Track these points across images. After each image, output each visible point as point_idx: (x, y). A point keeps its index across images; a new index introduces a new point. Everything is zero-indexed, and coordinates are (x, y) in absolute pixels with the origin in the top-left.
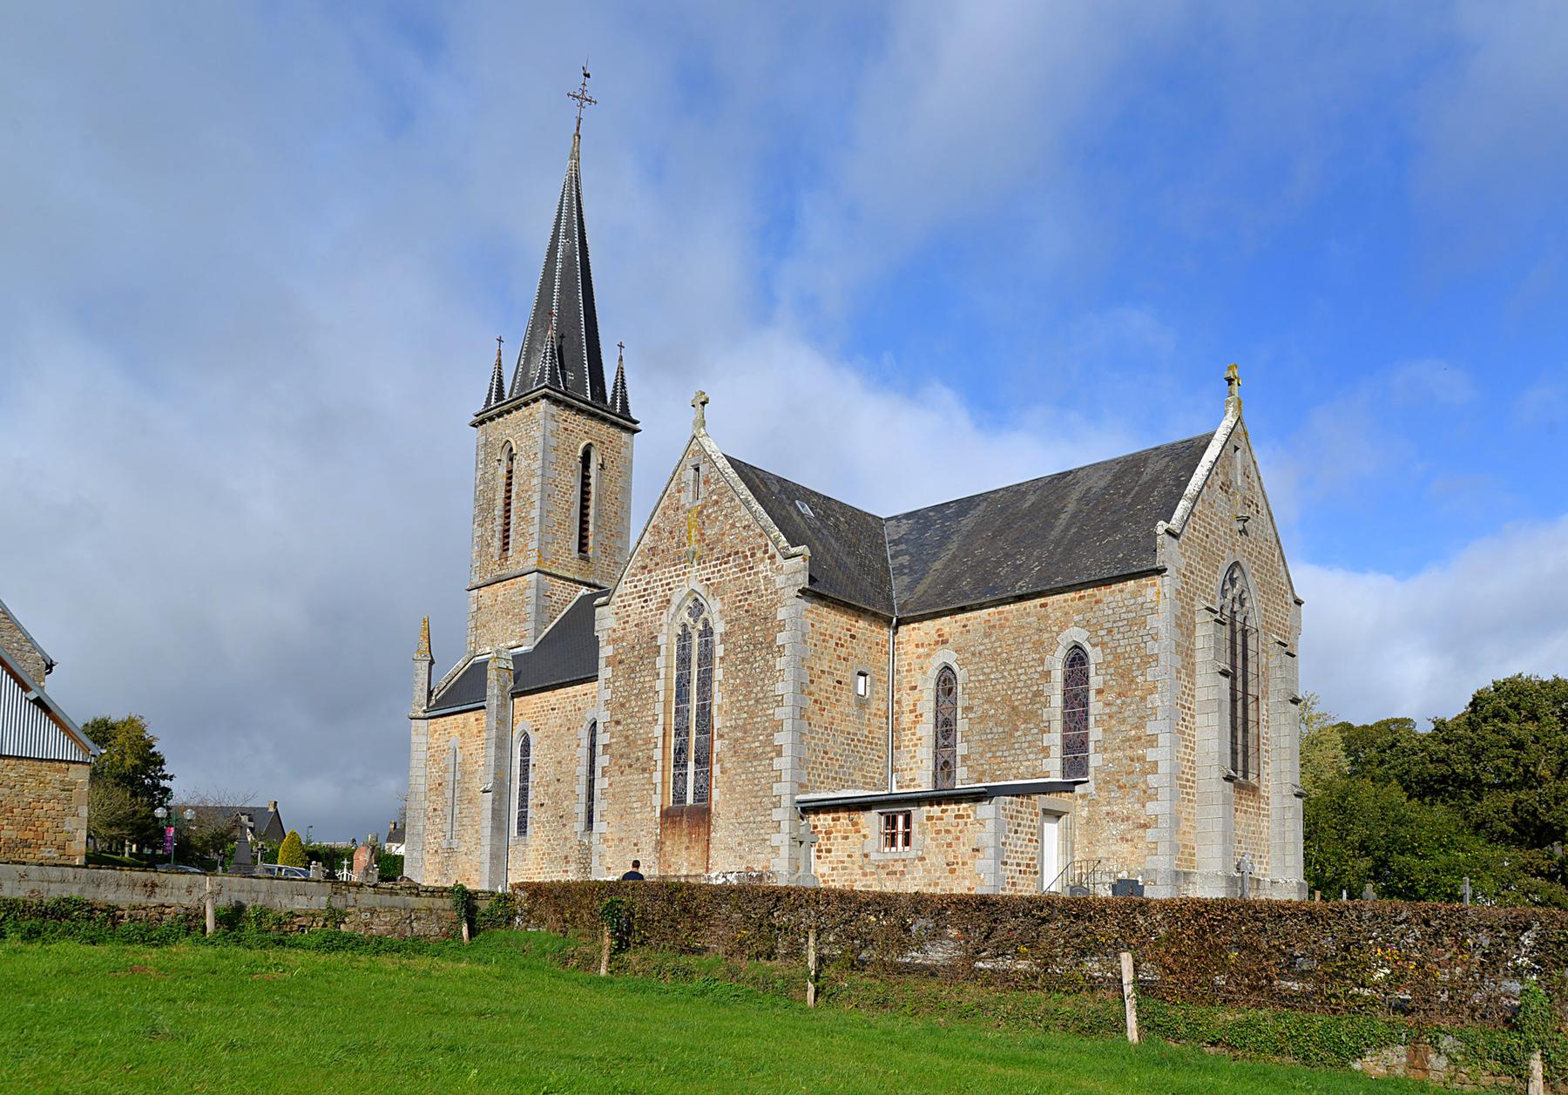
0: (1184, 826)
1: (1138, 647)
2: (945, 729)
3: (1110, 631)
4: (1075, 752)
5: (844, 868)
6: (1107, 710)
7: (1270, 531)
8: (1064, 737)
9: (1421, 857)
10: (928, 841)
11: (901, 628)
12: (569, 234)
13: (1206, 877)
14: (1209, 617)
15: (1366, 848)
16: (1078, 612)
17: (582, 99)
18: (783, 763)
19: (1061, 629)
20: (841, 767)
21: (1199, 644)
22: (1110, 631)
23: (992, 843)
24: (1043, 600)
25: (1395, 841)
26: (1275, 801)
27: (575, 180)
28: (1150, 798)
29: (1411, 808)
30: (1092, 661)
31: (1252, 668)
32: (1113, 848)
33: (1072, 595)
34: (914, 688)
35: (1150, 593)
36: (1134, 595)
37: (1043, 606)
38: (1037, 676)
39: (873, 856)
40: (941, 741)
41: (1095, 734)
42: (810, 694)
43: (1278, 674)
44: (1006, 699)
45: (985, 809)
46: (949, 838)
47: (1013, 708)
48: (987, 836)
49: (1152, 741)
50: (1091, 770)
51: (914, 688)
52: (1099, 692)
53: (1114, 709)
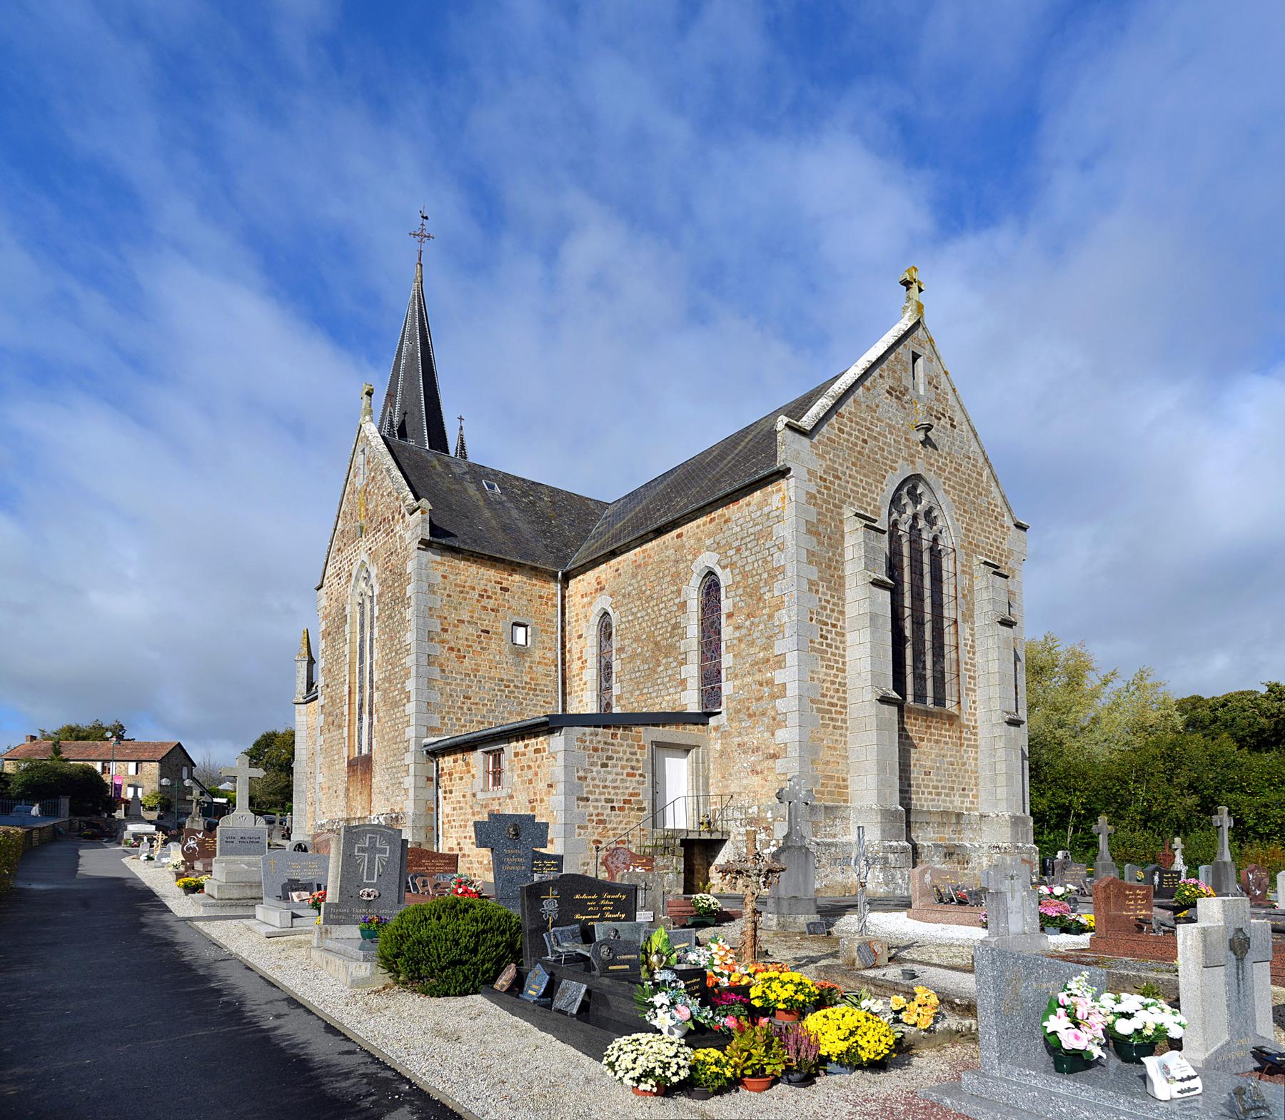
0: (825, 755)
1: (766, 562)
2: (605, 671)
3: (738, 549)
4: (711, 679)
5: (461, 808)
6: (737, 634)
7: (974, 447)
8: (702, 668)
9: (1251, 794)
10: (516, 778)
11: (572, 582)
12: (412, 338)
13: (860, 811)
14: (859, 524)
15: (1195, 788)
16: (709, 535)
17: (422, 236)
18: (411, 708)
19: (695, 557)
20: (490, 711)
21: (849, 555)
22: (738, 549)
23: (562, 778)
24: (678, 531)
25: (1223, 782)
26: (983, 733)
27: (421, 298)
28: (779, 726)
29: (1243, 756)
30: (722, 584)
31: (948, 589)
32: (745, 781)
33: (704, 519)
34: (580, 636)
35: (775, 501)
36: (760, 506)
37: (679, 536)
38: (675, 608)
39: (480, 795)
40: (604, 684)
41: (727, 660)
42: (443, 642)
43: (985, 596)
44: (651, 636)
45: (557, 742)
46: (530, 774)
47: (656, 644)
48: (556, 769)
49: (780, 662)
50: (724, 699)
51: (580, 636)
52: (730, 615)
53: (744, 631)
